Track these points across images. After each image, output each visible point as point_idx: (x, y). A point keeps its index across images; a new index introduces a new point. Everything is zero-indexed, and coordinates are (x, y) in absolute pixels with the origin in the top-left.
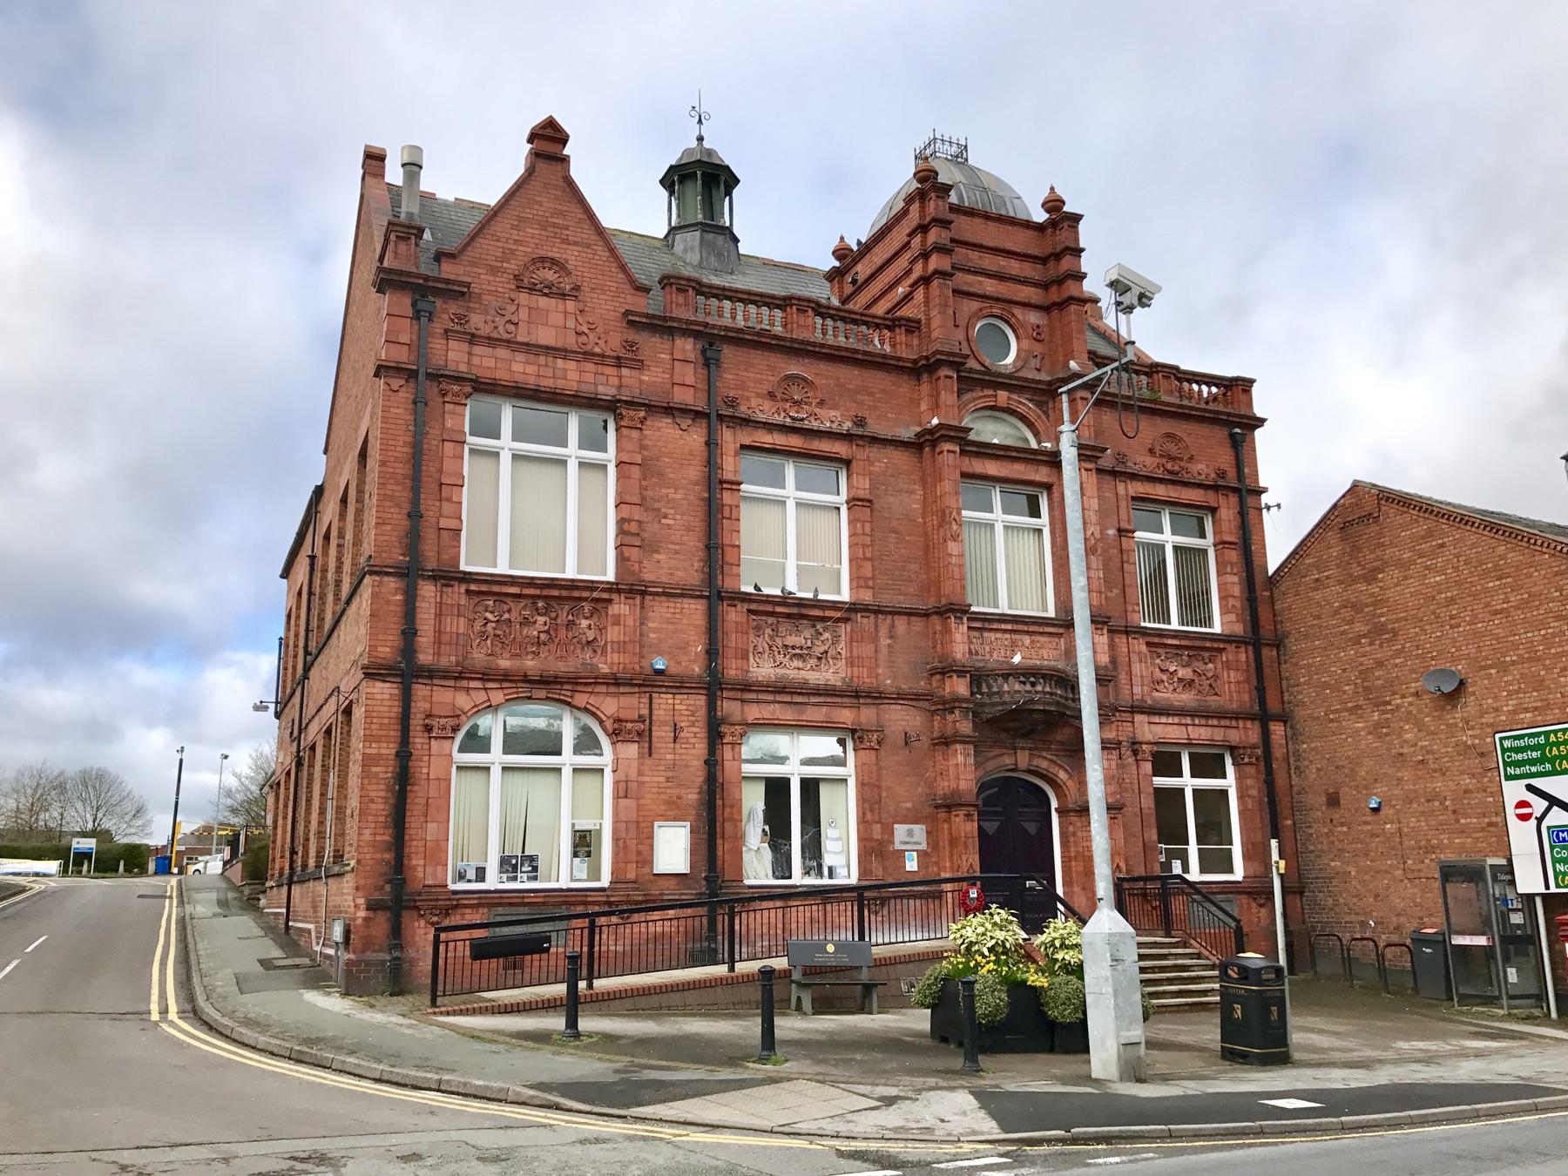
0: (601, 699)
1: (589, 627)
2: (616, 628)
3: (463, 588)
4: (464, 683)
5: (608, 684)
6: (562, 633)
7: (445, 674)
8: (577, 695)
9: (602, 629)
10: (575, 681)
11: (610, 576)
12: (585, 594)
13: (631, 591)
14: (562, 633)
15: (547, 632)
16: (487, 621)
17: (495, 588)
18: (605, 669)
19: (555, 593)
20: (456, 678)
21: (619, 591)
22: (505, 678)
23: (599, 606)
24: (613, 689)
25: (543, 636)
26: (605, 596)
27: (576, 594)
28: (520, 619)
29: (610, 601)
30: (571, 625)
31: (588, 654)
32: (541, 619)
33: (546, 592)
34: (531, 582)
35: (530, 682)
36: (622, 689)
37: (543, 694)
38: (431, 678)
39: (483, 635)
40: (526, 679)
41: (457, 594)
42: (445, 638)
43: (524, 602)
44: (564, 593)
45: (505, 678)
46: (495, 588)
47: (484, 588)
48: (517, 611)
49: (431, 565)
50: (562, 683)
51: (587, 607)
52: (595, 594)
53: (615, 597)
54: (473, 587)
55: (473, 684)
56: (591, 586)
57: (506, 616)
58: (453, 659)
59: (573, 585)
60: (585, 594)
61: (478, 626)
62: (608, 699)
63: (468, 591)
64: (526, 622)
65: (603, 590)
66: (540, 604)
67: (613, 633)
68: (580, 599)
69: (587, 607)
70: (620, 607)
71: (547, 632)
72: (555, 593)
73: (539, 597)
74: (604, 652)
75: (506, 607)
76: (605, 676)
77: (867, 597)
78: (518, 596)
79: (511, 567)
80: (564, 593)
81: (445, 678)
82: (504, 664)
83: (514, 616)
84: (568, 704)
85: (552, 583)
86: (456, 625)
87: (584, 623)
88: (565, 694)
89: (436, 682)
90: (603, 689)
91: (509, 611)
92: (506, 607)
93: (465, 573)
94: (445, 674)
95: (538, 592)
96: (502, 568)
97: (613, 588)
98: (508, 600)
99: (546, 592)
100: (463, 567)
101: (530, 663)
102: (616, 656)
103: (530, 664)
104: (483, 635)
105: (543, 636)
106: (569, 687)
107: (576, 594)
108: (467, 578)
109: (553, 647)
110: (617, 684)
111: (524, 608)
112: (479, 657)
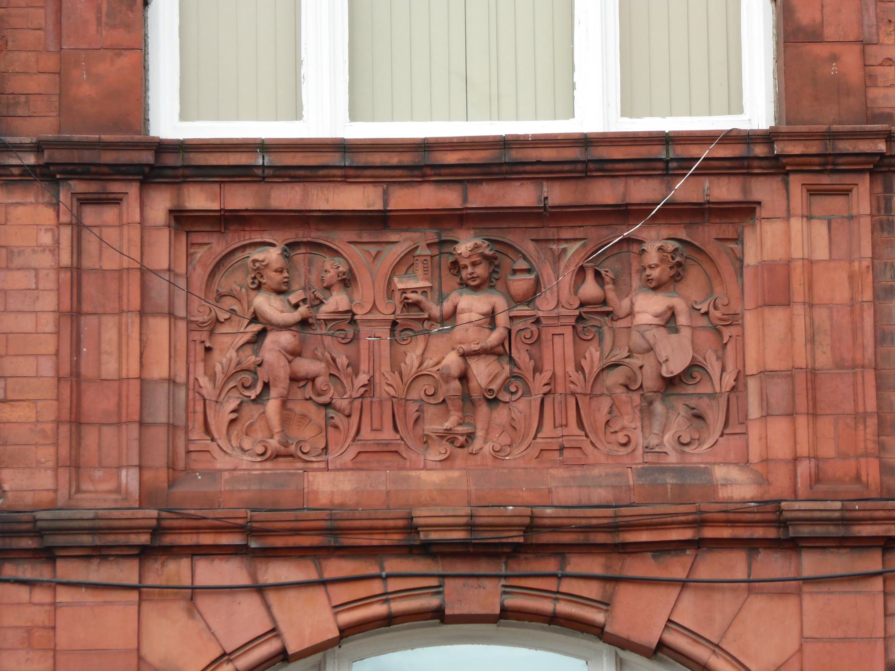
0: (724, 604)
1: (669, 321)
2: (777, 318)
3: (160, 204)
4: (177, 571)
5: (751, 546)
6: (560, 349)
7: (101, 541)
8: (626, 595)
9: (722, 326)
10: (613, 540)
11: (758, 112)
12: (643, 191)
13: (828, 163)
14: (560, 349)
15: (499, 353)
16: (264, 328)
17: (286, 197)
18: (736, 485)
19: (521, 195)
20: (144, 553)
21: (779, 167)
22: (329, 540)
23: (707, 234)
24: (773, 565)
25: (482, 372)
26: (725, 190)
27: (605, 193)
28: (386, 311)
29: (746, 211)
30: (591, 317)
31: (668, 429)
32: (472, 305)
33: (484, 196)
34: (421, 161)
35: (427, 550)
36: (811, 564)
37: (485, 596)
38: (48, 556)
39: (252, 383)
40: (414, 542)
41: (135, 229)
42: (98, 403)
43: (401, 242)
44: (558, 195)
45: (329, 540)
46: (286, 197)
47: (241, 198)
48: (380, 275)
49: (37, 125)
50: (560, 551)
51: (656, 242)
52: (682, 189)
53: (765, 190)
54: (199, 199)
55: (210, 572)
56: (660, 156)
57: (337, 301)
58: (130, 479)
59: (588, 158)
60: (643, 191)
61: (228, 349)
62: (758, 603)
63: (181, 219)
64: (411, 320)
65: (713, 169)
66: (466, 244)
67: (768, 339)
68: (625, 212)
69: (656, 242)
70: (789, 232)
71: (499, 353)
72: (521, 195)
73: (462, 218)
74: (734, 421)
75: (331, 267)
76: (733, 516)
77: (784, 128)
78: (379, 221)
79: (627, 111)
80: (558, 195)
81: (98, 554)
82: (332, 485)
83: (367, 298)
84: (598, 632)
85: (502, 160)
86: (131, 350)
87: (648, 307)
88: (579, 595)
89: (67, 570)
90: (735, 565)
91: (347, 281)
92: (331, 267)
93: (162, 147)
94: (101, 541)
95: (448, 198)
96: (324, 117)
97: (748, 156)
98: (339, 239)
99: (484, 196)
100: (167, 122)
101: (432, 478)
102: (779, 428)
103: (435, 484)
104: (252, 383)
105: (482, 372)
106: (594, 565)
107: (605, 193)
108: (170, 165)
109: (523, 408)
110: (792, 545)
111: (406, 262)
112: (234, 467)
